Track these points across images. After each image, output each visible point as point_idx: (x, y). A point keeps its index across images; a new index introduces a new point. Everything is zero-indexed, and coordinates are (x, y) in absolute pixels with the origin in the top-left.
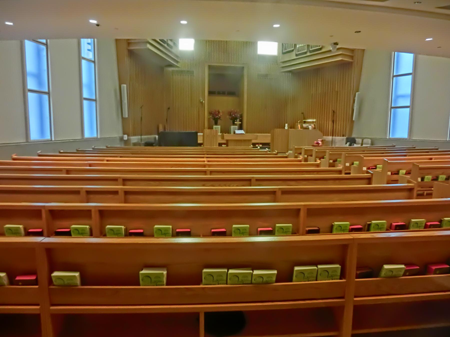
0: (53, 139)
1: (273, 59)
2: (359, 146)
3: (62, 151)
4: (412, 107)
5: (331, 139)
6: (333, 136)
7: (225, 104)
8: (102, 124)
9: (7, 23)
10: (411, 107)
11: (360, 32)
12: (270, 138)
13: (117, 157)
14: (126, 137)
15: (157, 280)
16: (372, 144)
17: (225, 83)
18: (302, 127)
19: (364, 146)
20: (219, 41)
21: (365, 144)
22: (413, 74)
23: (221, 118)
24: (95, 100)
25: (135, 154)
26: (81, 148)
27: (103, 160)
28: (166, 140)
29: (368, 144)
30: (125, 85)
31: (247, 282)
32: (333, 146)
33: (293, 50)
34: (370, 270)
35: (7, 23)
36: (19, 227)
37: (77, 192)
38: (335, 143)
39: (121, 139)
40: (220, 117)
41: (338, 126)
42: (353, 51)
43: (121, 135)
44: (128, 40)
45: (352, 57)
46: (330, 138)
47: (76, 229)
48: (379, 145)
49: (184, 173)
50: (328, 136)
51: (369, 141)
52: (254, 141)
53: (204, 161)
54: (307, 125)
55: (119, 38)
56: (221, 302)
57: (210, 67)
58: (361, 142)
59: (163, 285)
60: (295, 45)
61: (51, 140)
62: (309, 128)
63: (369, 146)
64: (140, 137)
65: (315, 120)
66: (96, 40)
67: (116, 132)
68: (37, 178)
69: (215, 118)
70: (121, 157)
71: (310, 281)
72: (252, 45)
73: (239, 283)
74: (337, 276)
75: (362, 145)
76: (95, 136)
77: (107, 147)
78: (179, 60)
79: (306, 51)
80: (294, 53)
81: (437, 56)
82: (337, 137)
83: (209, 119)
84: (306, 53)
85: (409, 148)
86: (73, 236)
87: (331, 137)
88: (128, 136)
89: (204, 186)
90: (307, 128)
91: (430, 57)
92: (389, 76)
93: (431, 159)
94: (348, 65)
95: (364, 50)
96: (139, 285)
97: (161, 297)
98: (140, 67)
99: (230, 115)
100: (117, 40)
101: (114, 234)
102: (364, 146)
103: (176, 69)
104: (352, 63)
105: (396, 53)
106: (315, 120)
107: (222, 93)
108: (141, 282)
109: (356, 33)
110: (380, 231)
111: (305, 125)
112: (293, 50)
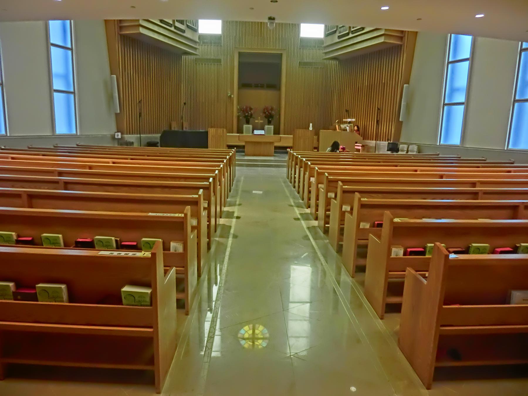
0: (8, 135)
1: (318, 42)
2: (405, 153)
3: (3, 147)
4: (467, 104)
5: (374, 145)
6: (376, 140)
7: (260, 98)
8: (82, 119)
10: (465, 103)
11: (277, 1)
12: (291, 141)
13: (127, 159)
14: (119, 135)
15: (55, 295)
16: (419, 151)
18: (340, 128)
19: (409, 153)
20: (252, 22)
21: (411, 151)
22: (470, 59)
23: (253, 116)
24: (74, 93)
25: (134, 156)
26: (58, 147)
27: (7, 158)
28: (173, 139)
29: (413, 152)
30: (115, 76)
31: (145, 304)
32: (377, 153)
33: (335, 32)
34: (25, 288)
36: (11, 235)
37: (17, 196)
38: (379, 149)
39: (113, 138)
40: (251, 115)
41: (384, 128)
42: (402, 32)
43: (113, 133)
44: (121, 21)
45: (401, 38)
46: (372, 143)
47: (100, 241)
48: (427, 152)
49: (138, 178)
50: (373, 140)
51: (415, 148)
52: (277, 144)
53: (108, 163)
54: (345, 125)
55: (105, 19)
56: (142, 325)
57: (240, 54)
58: (406, 149)
59: (63, 301)
60: (337, 26)
61: (7, 136)
62: (347, 130)
63: (415, 153)
64: (139, 135)
65: (354, 120)
66: (72, 21)
67: (105, 129)
68: (96, 182)
69: (246, 116)
70: (132, 159)
71: (7, 299)
72: (296, 27)
73: (136, 304)
74: (146, 302)
75: (407, 152)
76: (74, 132)
77: (77, 145)
78: (197, 47)
79: (347, 32)
80: (337, 34)
81: (497, 38)
82: (381, 142)
83: (238, 117)
84: (348, 34)
85: (458, 158)
86: (96, 249)
87: (374, 142)
88: (122, 134)
89: (13, 187)
90: (345, 130)
91: (497, 40)
92: (443, 63)
93: (416, 171)
94: (396, 48)
95: (417, 32)
96: (37, 301)
97: (58, 314)
99: (265, 113)
100: (106, 21)
101: (103, 246)
102: (409, 153)
103: (193, 57)
104: (401, 46)
105: (453, 35)
106: (354, 120)
107: (259, 86)
108: (124, 301)
109: (273, 3)
111: (343, 126)
112: (335, 32)
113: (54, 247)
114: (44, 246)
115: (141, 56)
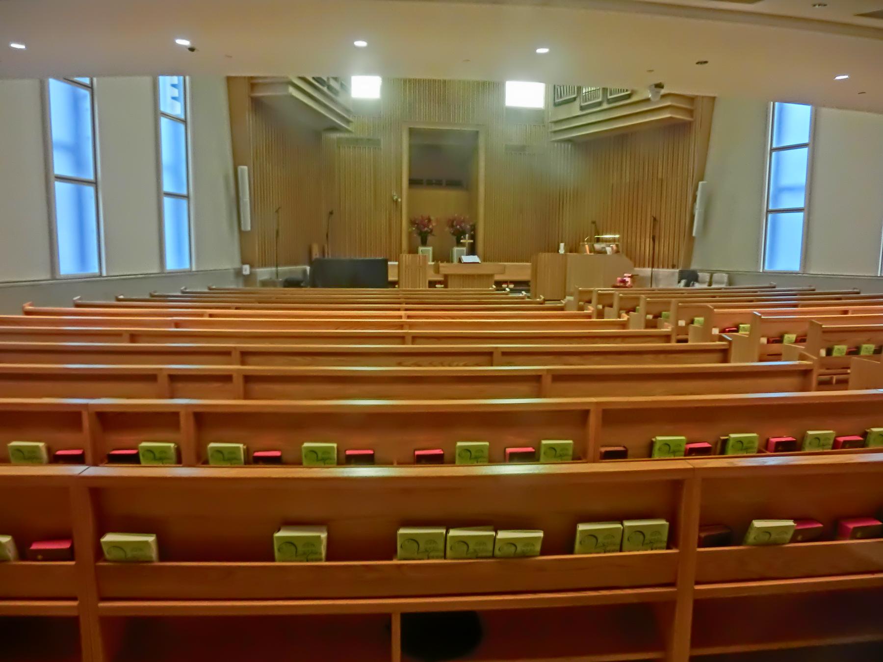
0: (104, 274)
1: (536, 116)
2: (705, 286)
3: (121, 297)
4: (808, 210)
5: (650, 274)
6: (653, 267)
7: (441, 204)
8: (200, 244)
9: (14, 45)
10: (806, 210)
11: (706, 62)
12: (529, 272)
13: (229, 308)
14: (246, 269)
15: (308, 549)
16: (730, 282)
18: (592, 250)
19: (714, 286)
20: (429, 81)
21: (717, 283)
22: (811, 145)
23: (434, 233)
24: (187, 197)
25: (264, 302)
26: (159, 290)
27: (201, 315)
28: (325, 275)
29: (721, 283)
30: (246, 168)
31: (484, 554)
32: (654, 287)
33: (575, 99)
35: (14, 45)
37: (151, 377)
38: (658, 281)
39: (238, 273)
40: (432, 231)
41: (663, 248)
42: (692, 99)
43: (237, 265)
44: (252, 78)
45: (691, 112)
46: (647, 271)
48: (743, 284)
49: (362, 340)
50: (644, 266)
51: (725, 277)
52: (498, 278)
53: (400, 317)
54: (603, 245)
55: (233, 74)
56: (433, 592)
57: (412, 132)
58: (708, 279)
59: (320, 560)
60: (579, 89)
61: (101, 276)
62: (605, 252)
63: (723, 286)
64: (274, 269)
65: (617, 236)
66: (187, 78)
67: (227, 260)
68: (74, 349)
69: (422, 232)
70: (237, 308)
71: (609, 551)
72: (494, 87)
73: (469, 556)
74: (661, 542)
75: (710, 285)
76: (187, 266)
77: (210, 289)
78: (351, 119)
79: (600, 100)
80: (577, 104)
81: (857, 110)
82: (661, 270)
83: (410, 235)
84: (600, 104)
85: (804, 291)
87: (650, 269)
88: (252, 266)
89: (400, 364)
90: (603, 252)
91: (844, 111)
92: (763, 149)
93: (846, 312)
94: (683, 127)
96: (273, 560)
97: (315, 583)
99: (452, 226)
100: (229, 79)
101: (224, 460)
102: (714, 286)
103: (346, 135)
104: (690, 123)
105: (777, 104)
106: (617, 236)
107: (436, 183)
108: (277, 554)
109: (699, 65)
111: (598, 246)
112: (575, 99)
113: (745, 454)
114: (807, 451)
115: (275, 132)
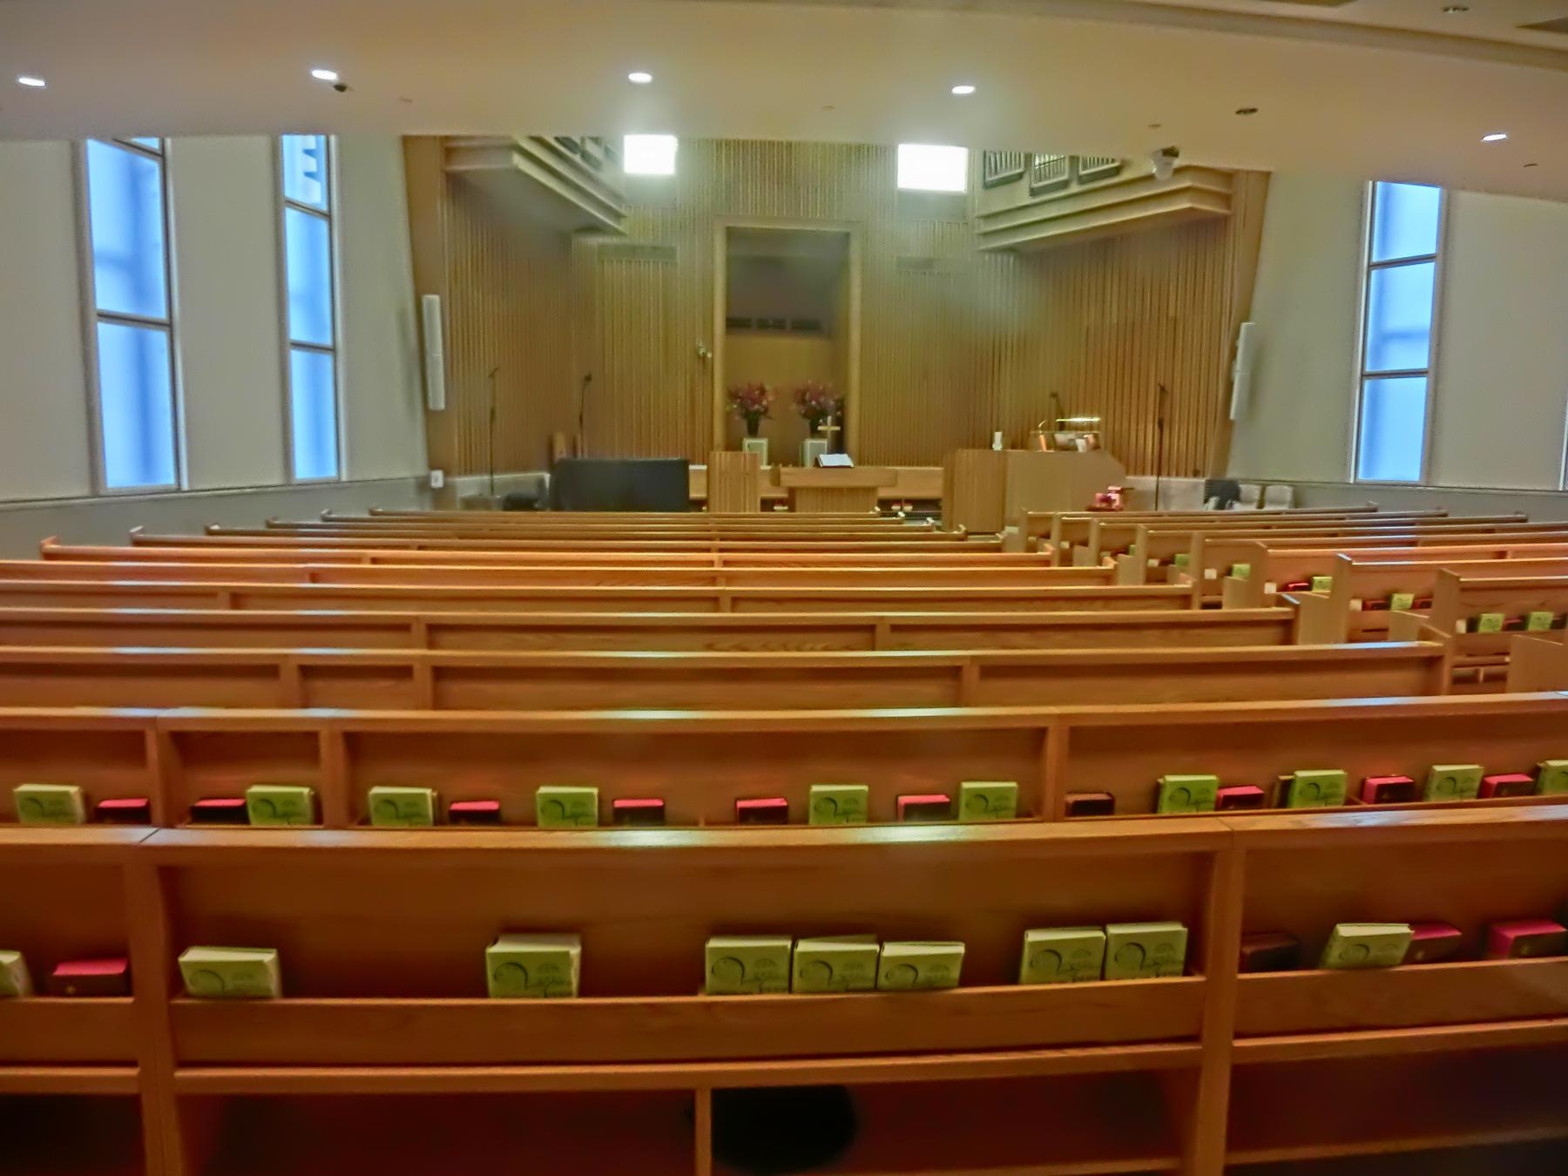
0: (185, 486)
1: (953, 206)
2: (1252, 508)
3: (216, 527)
4: (1435, 373)
5: (1154, 487)
6: (1159, 474)
7: (783, 362)
8: (355, 433)
9: (25, 81)
10: (1431, 373)
11: (1253, 110)
12: (939, 483)
13: (406, 547)
14: (438, 478)
15: (546, 976)
16: (1297, 502)
17: (782, 289)
18: (1052, 444)
19: (1267, 508)
20: (763, 143)
21: (1273, 502)
22: (1440, 258)
23: (770, 413)
24: (333, 350)
25: (470, 536)
26: (282, 516)
27: (358, 560)
28: (577, 488)
29: (1281, 503)
30: (436, 298)
31: (860, 985)
32: (1161, 510)
33: (1020, 176)
34: (1289, 942)
35: (25, 81)
36: (66, 794)
37: (267, 671)
38: (1168, 499)
39: (423, 485)
40: (766, 410)
41: (1178, 441)
42: (1228, 176)
43: (421, 470)
44: (447, 138)
45: (1226, 199)
46: (1149, 482)
47: (266, 800)
48: (1319, 505)
49: (642, 604)
50: (1143, 473)
51: (1287, 492)
52: (884, 493)
53: (711, 563)
54: (1071, 435)
55: (413, 132)
56: (769, 1052)
57: (732, 235)
58: (1256, 496)
59: (569, 995)
60: (1029, 158)
61: (179, 490)
62: (1075, 448)
63: (1284, 508)
64: (486, 478)
65: (1096, 419)
66: (333, 139)
67: (403, 461)
68: (131, 620)
69: (749, 412)
70: (421, 548)
71: (1082, 980)
72: (878, 155)
73: (832, 987)
74: (1174, 962)
75: (1261, 506)
76: (331, 473)
77: (373, 513)
78: (623, 211)
79: (1065, 177)
80: (1024, 185)
81: (1522, 195)
82: (1173, 479)
83: (728, 417)
84: (1065, 184)
85: (1427, 517)
86: (253, 825)
87: (1154, 478)
88: (447, 473)
89: (710, 647)
90: (1070, 448)
91: (1500, 198)
92: (1355, 264)
93: (1502, 554)
94: (1213, 225)
95: (1267, 175)
96: (485, 995)
97: (560, 1036)
98: (489, 235)
99: (803, 402)
100: (407, 140)
101: (398, 817)
102: (1267, 508)
103: (614, 240)
104: (1225, 218)
105: (1379, 184)
106: (1096, 419)
107: (774, 326)
108: (491, 984)
109: (1242, 116)
110: (1323, 807)
111: (1061, 437)
112: (1020, 176)
